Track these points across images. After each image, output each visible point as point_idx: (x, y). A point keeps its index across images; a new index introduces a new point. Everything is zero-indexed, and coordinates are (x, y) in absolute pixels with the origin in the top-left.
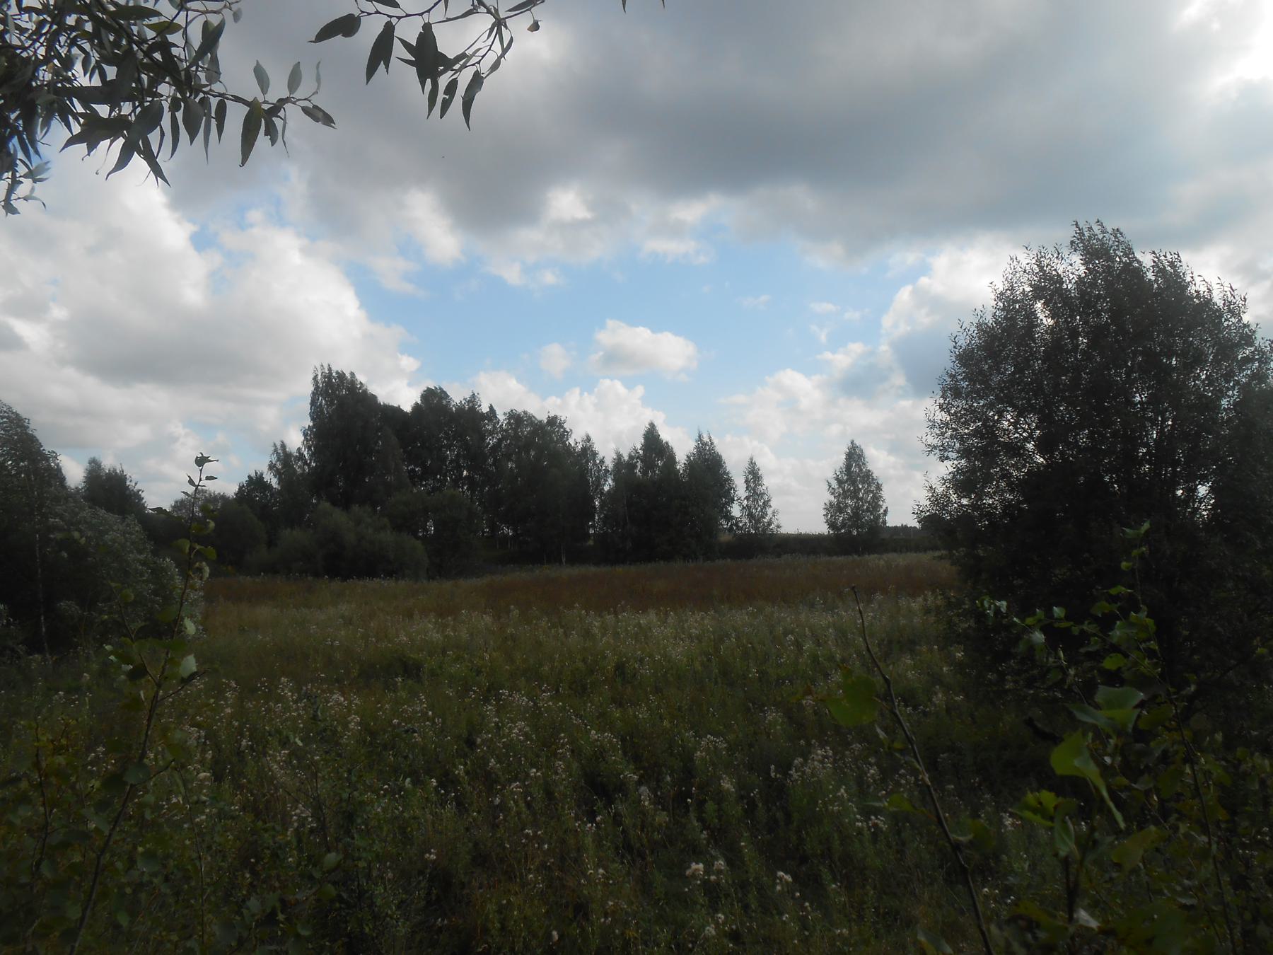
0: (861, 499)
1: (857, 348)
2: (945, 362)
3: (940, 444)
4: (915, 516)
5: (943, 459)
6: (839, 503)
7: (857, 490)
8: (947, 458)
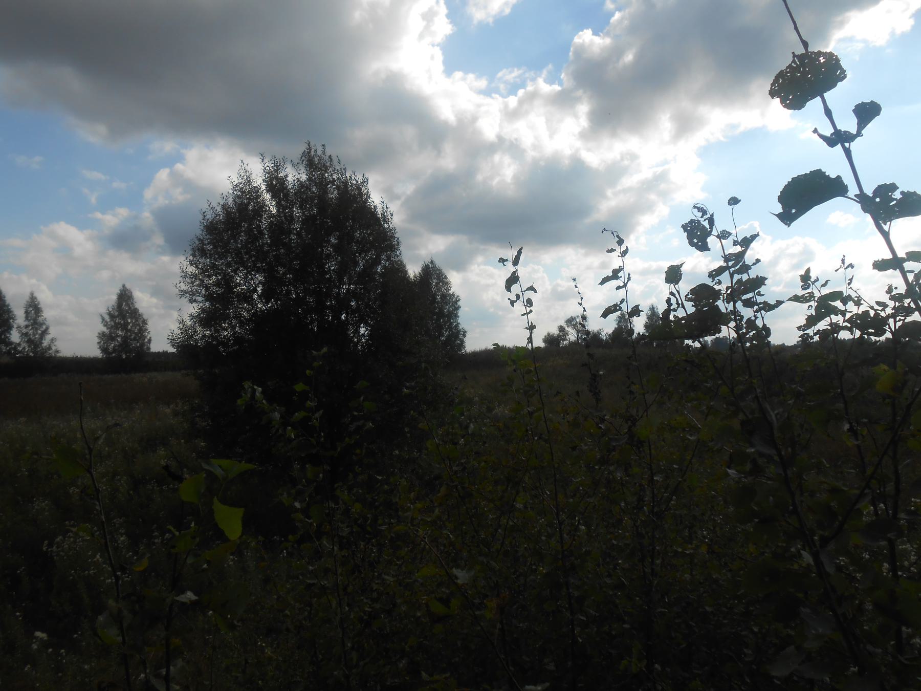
0: (130, 331)
1: (123, 212)
2: (196, 230)
3: (190, 290)
4: (169, 341)
5: (191, 301)
6: (111, 333)
7: (127, 324)
8: (195, 301)
